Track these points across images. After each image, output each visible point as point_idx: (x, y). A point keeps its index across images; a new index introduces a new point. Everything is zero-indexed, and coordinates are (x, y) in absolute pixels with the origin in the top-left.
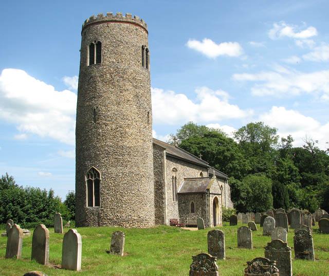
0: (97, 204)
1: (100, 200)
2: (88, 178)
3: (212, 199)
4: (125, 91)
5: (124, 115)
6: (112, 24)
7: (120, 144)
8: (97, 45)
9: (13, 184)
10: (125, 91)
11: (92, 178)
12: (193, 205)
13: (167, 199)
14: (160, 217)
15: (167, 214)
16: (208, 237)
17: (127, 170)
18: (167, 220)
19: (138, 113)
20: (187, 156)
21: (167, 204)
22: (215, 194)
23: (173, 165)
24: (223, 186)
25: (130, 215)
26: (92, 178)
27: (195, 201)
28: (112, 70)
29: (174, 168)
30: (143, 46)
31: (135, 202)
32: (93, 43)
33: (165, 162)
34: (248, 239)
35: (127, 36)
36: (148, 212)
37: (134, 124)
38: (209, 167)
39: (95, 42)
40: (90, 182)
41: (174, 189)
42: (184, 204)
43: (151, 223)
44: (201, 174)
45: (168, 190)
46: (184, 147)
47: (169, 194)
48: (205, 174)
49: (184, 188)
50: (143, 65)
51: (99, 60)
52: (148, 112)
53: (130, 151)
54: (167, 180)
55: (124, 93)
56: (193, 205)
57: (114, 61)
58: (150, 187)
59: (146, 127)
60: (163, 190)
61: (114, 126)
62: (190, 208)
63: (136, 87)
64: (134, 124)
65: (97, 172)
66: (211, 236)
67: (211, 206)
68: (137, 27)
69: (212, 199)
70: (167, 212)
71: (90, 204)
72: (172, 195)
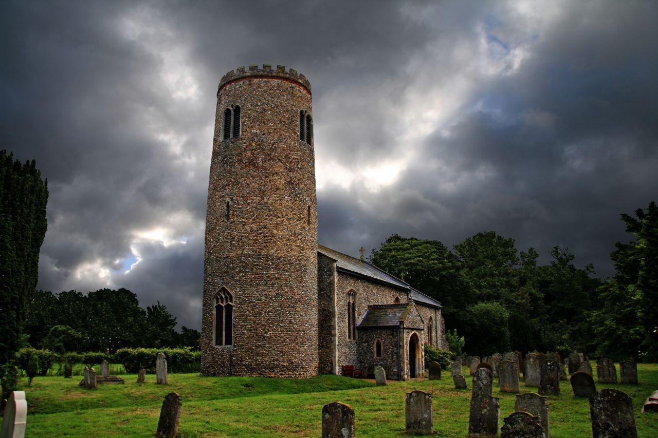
0: (228, 342)
1: (233, 335)
2: (217, 302)
3: (407, 337)
4: (273, 174)
5: (270, 210)
6: (256, 80)
7: (264, 252)
8: (234, 110)
9: (166, 314)
10: (273, 174)
11: (222, 302)
12: (379, 345)
13: (337, 335)
14: (325, 367)
15: (337, 358)
16: (323, 417)
17: (273, 292)
18: (337, 368)
19: (292, 208)
20: (382, 278)
21: (337, 343)
22: (413, 329)
23: (350, 285)
24: (433, 318)
25: (277, 360)
26: (222, 302)
27: (382, 339)
28: (254, 145)
29: (351, 291)
30: (301, 112)
31: (285, 340)
32: (231, 108)
33: (336, 280)
34: (426, 416)
35: (279, 98)
36: (308, 353)
37: (286, 222)
38: (410, 290)
39: (232, 106)
40: (219, 308)
41: (351, 322)
42: (366, 344)
43: (312, 370)
44: (397, 299)
45: (339, 322)
46: (376, 263)
47: (340, 328)
48: (403, 299)
49: (81, 276)
50: (302, 138)
51: (236, 133)
52: (309, 207)
53: (280, 263)
54: (339, 305)
55: (271, 178)
56: (379, 345)
57: (258, 132)
58: (313, 317)
59: (304, 228)
60: (332, 324)
61: (254, 226)
62: (375, 349)
63: (290, 170)
64: (286, 222)
65: (229, 293)
66: (327, 416)
67: (407, 348)
68: (294, 85)
69: (407, 337)
70: (337, 356)
71: (219, 342)
72: (347, 331)
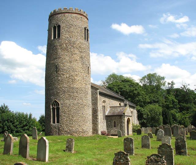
0: (58, 122)
1: (60, 119)
2: (53, 106)
3: (126, 119)
4: (75, 54)
5: (74, 69)
6: (67, 14)
7: (72, 86)
8: (58, 27)
9: (8, 110)
10: (75, 54)
11: (55, 106)
12: (115, 122)
13: (99, 119)
14: (95, 130)
15: (99, 128)
16: (124, 142)
17: (76, 102)
18: (99, 132)
19: (82, 68)
20: (111, 93)
21: (99, 122)
22: (128, 116)
23: (103, 99)
24: (133, 111)
25: (78, 129)
26: (55, 106)
27: (116, 120)
28: (67, 42)
29: (104, 101)
30: (85, 28)
31: (80, 121)
32: (56, 25)
33: (98, 97)
34: (148, 143)
35: (76, 22)
36: (88, 127)
37: (80, 74)
38: (124, 100)
39: (57, 25)
40: (53, 109)
41: (104, 113)
42: (110, 122)
43: (90, 134)
44: (120, 104)
45: (100, 113)
46: (109, 88)
47: (100, 116)
48: (122, 104)
49: (110, 112)
50: (85, 39)
51: (59, 36)
52: (88, 67)
53: (77, 90)
54: (100, 108)
55: (74, 56)
56: (115, 122)
57: (68, 36)
58: (90, 112)
59: (87, 76)
60: (97, 114)
61: (68, 76)
62: (113, 124)
63: (81, 52)
64: (80, 74)
65: (58, 103)
66: (125, 141)
67: (126, 123)
68: (82, 16)
69: (126, 119)
70: (99, 127)
71: (54, 122)
72: (102, 117)
